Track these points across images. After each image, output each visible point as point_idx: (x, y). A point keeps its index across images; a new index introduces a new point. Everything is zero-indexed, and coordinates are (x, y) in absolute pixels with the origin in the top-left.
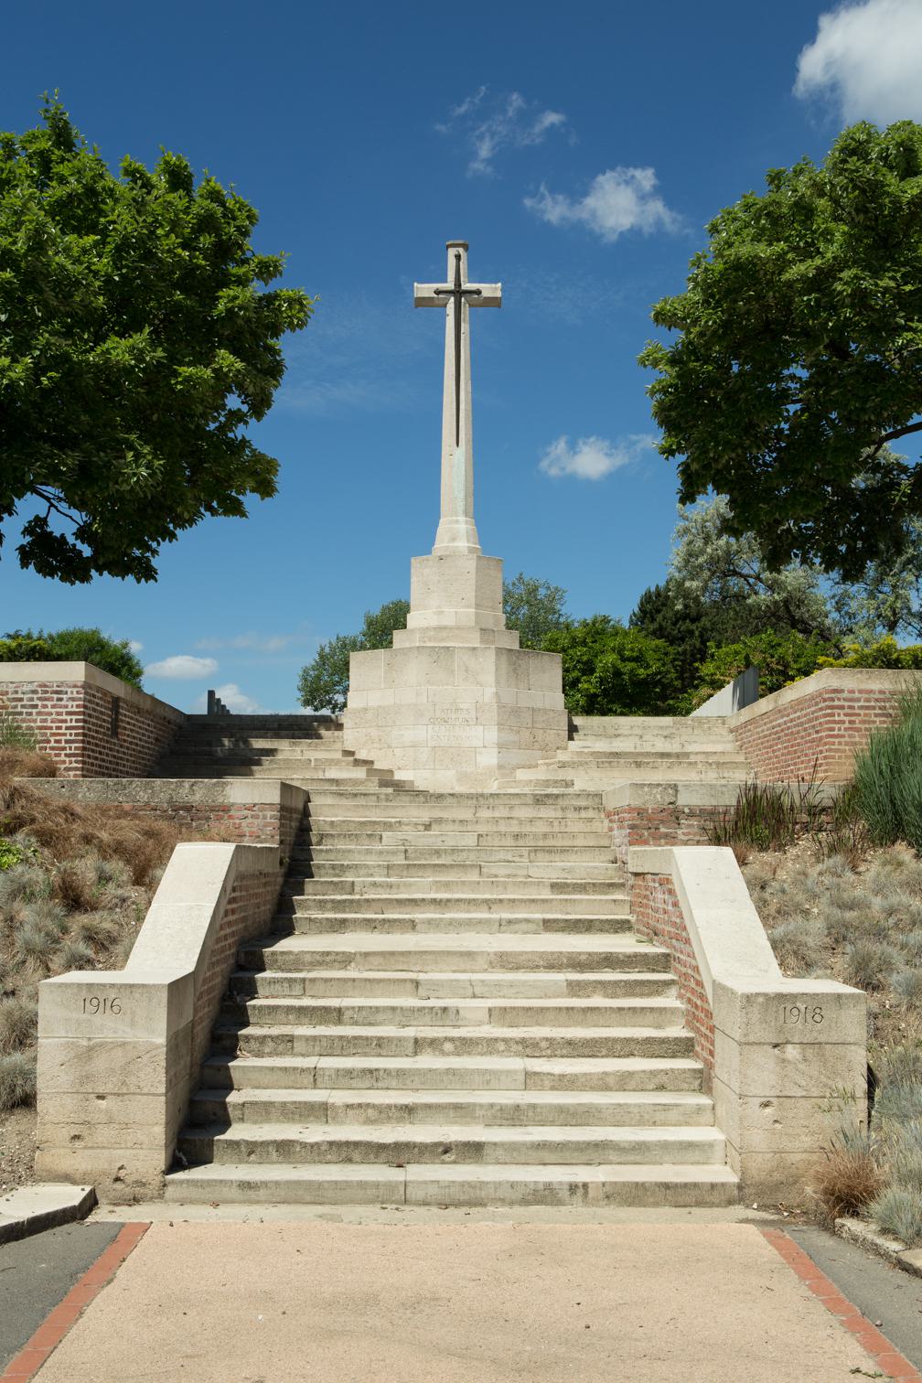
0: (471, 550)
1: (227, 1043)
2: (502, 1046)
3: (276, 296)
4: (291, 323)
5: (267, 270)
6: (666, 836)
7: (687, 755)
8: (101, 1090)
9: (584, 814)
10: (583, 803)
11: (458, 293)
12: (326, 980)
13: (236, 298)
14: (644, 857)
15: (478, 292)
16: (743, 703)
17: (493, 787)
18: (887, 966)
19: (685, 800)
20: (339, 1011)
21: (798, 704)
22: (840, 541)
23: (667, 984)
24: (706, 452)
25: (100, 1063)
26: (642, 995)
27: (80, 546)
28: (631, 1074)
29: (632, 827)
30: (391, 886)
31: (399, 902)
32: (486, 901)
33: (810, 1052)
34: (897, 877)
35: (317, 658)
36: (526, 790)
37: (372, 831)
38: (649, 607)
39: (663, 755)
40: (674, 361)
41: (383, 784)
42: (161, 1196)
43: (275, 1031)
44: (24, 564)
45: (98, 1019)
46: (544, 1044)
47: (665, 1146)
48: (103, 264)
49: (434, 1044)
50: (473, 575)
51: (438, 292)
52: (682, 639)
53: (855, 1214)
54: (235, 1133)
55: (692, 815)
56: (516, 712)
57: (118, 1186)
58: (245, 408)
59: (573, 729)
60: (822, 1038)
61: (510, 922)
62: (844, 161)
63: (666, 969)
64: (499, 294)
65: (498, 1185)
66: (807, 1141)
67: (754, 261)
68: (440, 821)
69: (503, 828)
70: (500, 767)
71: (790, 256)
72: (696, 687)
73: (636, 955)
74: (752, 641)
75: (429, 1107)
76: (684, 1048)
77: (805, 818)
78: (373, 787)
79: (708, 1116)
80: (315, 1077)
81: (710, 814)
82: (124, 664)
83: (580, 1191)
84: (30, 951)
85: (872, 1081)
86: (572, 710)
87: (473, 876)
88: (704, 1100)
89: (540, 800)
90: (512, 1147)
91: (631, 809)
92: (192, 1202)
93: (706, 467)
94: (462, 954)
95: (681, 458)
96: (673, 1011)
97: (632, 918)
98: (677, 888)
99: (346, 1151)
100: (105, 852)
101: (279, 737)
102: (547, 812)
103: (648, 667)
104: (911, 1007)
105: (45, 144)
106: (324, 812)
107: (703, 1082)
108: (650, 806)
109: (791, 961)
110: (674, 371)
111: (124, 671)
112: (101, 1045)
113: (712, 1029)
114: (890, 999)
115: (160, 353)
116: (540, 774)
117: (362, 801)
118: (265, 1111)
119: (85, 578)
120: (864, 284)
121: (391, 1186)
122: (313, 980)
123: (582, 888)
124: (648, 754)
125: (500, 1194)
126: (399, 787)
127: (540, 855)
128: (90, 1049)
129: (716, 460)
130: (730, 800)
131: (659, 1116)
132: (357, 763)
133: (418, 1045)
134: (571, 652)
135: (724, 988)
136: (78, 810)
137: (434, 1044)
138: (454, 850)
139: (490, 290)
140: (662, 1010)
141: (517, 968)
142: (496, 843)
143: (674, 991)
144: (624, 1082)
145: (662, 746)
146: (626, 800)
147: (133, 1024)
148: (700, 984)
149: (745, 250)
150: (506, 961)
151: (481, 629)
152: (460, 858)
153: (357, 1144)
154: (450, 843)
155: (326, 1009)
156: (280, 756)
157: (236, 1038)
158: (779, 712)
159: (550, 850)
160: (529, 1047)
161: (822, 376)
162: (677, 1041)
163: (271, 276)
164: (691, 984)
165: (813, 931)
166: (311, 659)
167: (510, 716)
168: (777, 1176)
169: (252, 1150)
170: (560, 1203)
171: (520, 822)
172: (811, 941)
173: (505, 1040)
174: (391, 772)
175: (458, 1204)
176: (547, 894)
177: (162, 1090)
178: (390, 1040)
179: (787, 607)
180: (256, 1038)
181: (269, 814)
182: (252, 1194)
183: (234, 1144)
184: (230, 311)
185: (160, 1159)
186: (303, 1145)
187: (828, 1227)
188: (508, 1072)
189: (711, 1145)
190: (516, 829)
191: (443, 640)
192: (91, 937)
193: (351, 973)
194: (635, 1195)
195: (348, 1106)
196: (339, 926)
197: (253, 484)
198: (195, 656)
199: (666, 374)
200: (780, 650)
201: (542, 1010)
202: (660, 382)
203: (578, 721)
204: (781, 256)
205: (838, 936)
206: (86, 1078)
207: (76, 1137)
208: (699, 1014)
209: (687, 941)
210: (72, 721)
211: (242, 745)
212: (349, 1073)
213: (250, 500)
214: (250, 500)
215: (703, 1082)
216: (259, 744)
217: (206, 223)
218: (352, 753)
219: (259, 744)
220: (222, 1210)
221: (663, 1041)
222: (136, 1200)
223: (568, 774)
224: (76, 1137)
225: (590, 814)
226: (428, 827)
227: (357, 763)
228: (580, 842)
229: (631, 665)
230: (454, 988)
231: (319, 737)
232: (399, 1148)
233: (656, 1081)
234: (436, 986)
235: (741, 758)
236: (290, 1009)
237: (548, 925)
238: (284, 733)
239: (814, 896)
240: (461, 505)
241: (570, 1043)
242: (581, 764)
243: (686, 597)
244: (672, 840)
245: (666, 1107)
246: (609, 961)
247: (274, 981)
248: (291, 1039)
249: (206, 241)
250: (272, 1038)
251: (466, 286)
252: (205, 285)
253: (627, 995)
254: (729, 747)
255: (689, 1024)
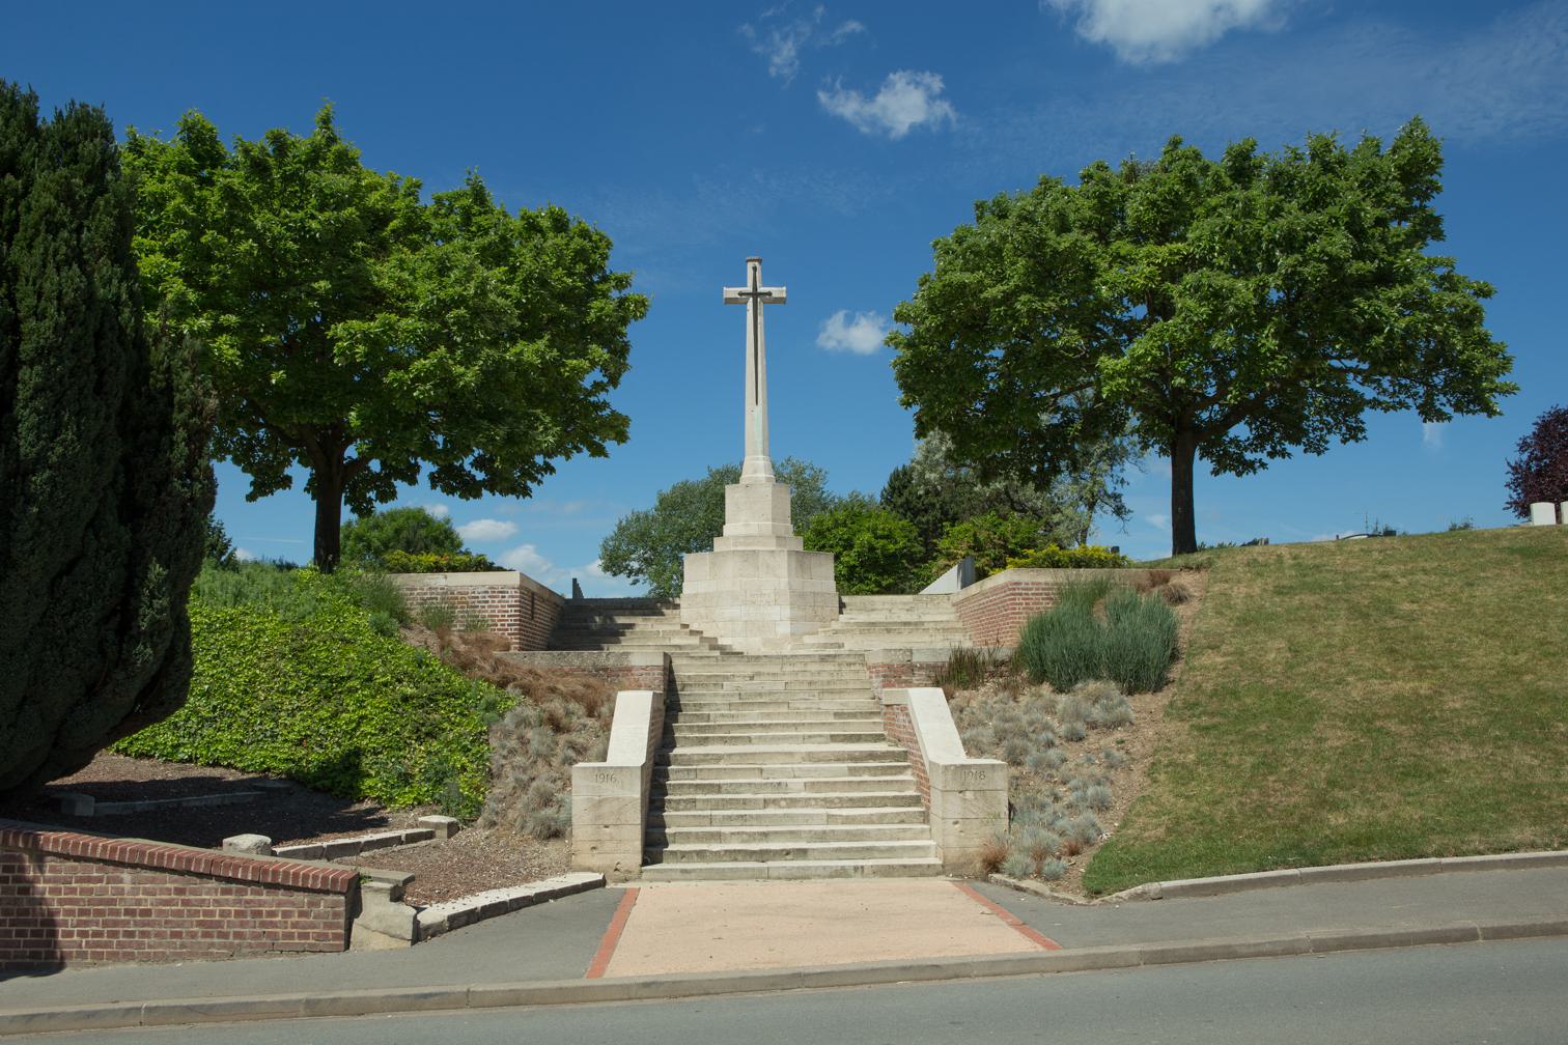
0: (768, 480)
1: (658, 804)
2: (813, 803)
3: (626, 299)
4: (635, 315)
5: (622, 283)
6: (906, 681)
7: (922, 623)
8: (606, 823)
9: (853, 668)
10: (852, 660)
11: (755, 294)
12: (710, 770)
13: (602, 309)
14: (891, 695)
15: (770, 294)
16: (965, 584)
17: (787, 650)
18: (1025, 751)
19: (917, 659)
20: (719, 786)
21: (995, 590)
22: (1032, 463)
23: (905, 768)
24: (933, 409)
25: (606, 809)
26: (891, 774)
27: (474, 472)
28: (886, 815)
29: (884, 676)
30: (733, 716)
31: (739, 726)
32: (794, 724)
33: (978, 794)
34: (1040, 703)
35: (616, 529)
36: (811, 652)
37: (717, 681)
38: (897, 483)
39: (906, 624)
40: (910, 345)
41: (713, 647)
42: (640, 878)
43: (684, 797)
44: (434, 487)
45: (604, 785)
46: (837, 801)
47: (904, 848)
48: (513, 289)
49: (775, 802)
50: (770, 498)
51: (741, 294)
52: (926, 511)
53: (998, 871)
54: (671, 847)
55: (921, 668)
56: (802, 595)
57: (617, 873)
58: (606, 380)
59: (842, 606)
60: (985, 788)
61: (810, 737)
62: (1019, 224)
63: (905, 760)
64: (784, 295)
65: (817, 868)
66: (977, 841)
67: (963, 286)
68: (759, 674)
69: (801, 679)
70: (792, 634)
71: (986, 281)
72: (935, 559)
73: (888, 752)
74: (978, 521)
75: (776, 833)
76: (916, 801)
77: (992, 668)
78: (706, 652)
79: (927, 835)
80: (711, 820)
81: (933, 667)
82: (447, 538)
83: (860, 871)
84: (539, 755)
85: (1011, 807)
86: (841, 591)
87: (784, 709)
88: (926, 826)
89: (824, 659)
90: (823, 851)
91: (883, 665)
92: (657, 880)
93: (933, 419)
94: (786, 753)
95: (916, 408)
96: (909, 782)
97: (886, 733)
98: (910, 711)
99: (733, 855)
100: (566, 697)
101: (633, 615)
102: (829, 667)
103: (896, 543)
104: (1036, 773)
105: (468, 201)
106: (683, 670)
107: (925, 817)
108: (895, 663)
109: (973, 750)
110: (909, 353)
111: (447, 543)
112: (606, 799)
113: (929, 788)
114: (1026, 769)
115: (555, 353)
116: (821, 639)
117: (705, 662)
118: (687, 837)
119: (478, 495)
120: (1035, 306)
121: (761, 870)
122: (701, 770)
123: (853, 715)
124: (895, 623)
125: (819, 872)
126: (727, 653)
127: (826, 695)
128: (600, 802)
129: (940, 414)
130: (945, 658)
131: (901, 835)
132: (692, 633)
133: (766, 802)
134: (834, 531)
135: (934, 764)
136: (539, 672)
137: (775, 802)
138: (771, 693)
139: (778, 292)
140: (903, 782)
141: (819, 761)
142: (797, 687)
143: (909, 772)
144: (881, 819)
145: (905, 617)
146: (880, 659)
147: (623, 788)
148: (923, 764)
149: (958, 277)
150: (812, 757)
151: (778, 537)
152: (774, 698)
153: (739, 851)
154: (767, 688)
155: (712, 785)
156: (637, 629)
157: (663, 801)
158: (983, 594)
159: (832, 692)
160: (828, 802)
161: (1013, 353)
162: (911, 797)
163: (624, 287)
164: (919, 768)
165: (986, 734)
166: (610, 530)
167: (799, 598)
168: (962, 860)
169: (684, 855)
170: (849, 876)
171: (812, 674)
172: (984, 740)
173: (815, 799)
174: (716, 639)
175: (796, 878)
176: (831, 720)
177: (639, 822)
178: (750, 800)
179: (1007, 493)
180: (675, 801)
181: (656, 672)
182: (688, 876)
183: (672, 852)
184: (599, 318)
185: (638, 859)
186: (711, 852)
187: (986, 880)
188: (817, 815)
189: (928, 847)
190: (809, 678)
191: (749, 545)
192: (572, 746)
193: (722, 765)
194: (888, 872)
195: (733, 833)
196: (704, 741)
197: (614, 435)
198: (497, 520)
199: (903, 353)
200: (1002, 528)
201: (835, 783)
202: (899, 358)
203: (845, 599)
204: (980, 282)
205: (1000, 737)
206: (599, 817)
207: (594, 848)
208: (923, 782)
209: (916, 742)
210: (512, 611)
211: (608, 621)
212: (730, 817)
213: (610, 445)
214: (610, 445)
215: (925, 817)
216: (621, 620)
217: (581, 255)
218: (685, 626)
219: (621, 620)
220: (673, 883)
221: (903, 797)
222: (626, 880)
223: (840, 639)
224: (594, 848)
225: (857, 667)
226: (752, 678)
227: (692, 633)
228: (851, 686)
229: (882, 542)
230: (782, 772)
231: (663, 614)
232: (762, 852)
233: (899, 818)
234: (774, 771)
235: (960, 625)
236: (690, 785)
237: (834, 738)
238: (637, 612)
239: (991, 717)
240: (760, 447)
241: (851, 800)
242: (848, 631)
243: (926, 484)
244: (909, 684)
245: (904, 830)
246: (872, 756)
247: (678, 771)
248: (694, 801)
249: (580, 268)
250: (684, 801)
251: (761, 289)
252: (579, 299)
253: (882, 774)
254: (952, 617)
255: (918, 789)
